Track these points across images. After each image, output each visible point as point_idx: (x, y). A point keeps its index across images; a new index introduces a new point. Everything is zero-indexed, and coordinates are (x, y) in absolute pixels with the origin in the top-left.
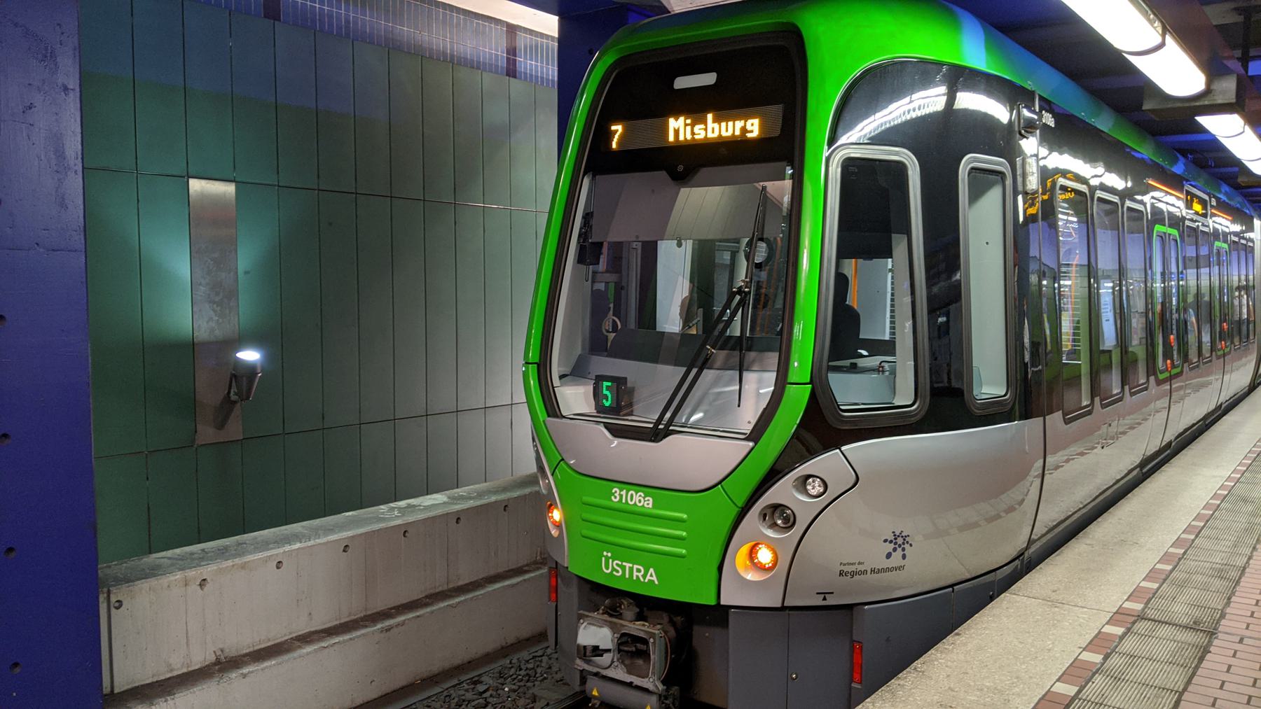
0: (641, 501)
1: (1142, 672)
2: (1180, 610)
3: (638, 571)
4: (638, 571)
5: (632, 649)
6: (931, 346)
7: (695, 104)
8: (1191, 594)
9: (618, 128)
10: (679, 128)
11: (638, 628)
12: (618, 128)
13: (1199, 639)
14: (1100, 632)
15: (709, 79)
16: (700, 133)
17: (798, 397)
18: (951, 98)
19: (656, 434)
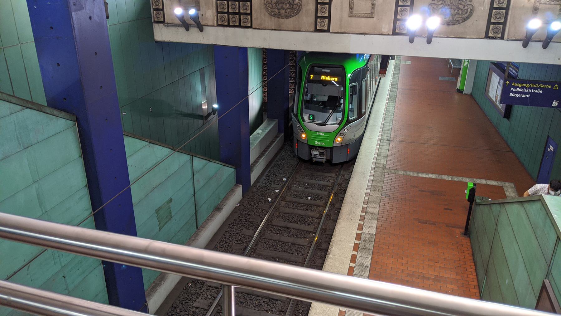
0: (321, 134)
1: (384, 147)
2: (385, 138)
3: (321, 144)
4: (321, 144)
5: (321, 154)
6: (41, 67)
7: (327, 74)
8: (386, 135)
9: (312, 76)
10: (323, 77)
11: (322, 151)
12: (312, 76)
13: (388, 142)
14: (218, 25)
15: (328, 71)
16: (327, 79)
17: (346, 119)
18: (424, 21)
19: (324, 125)
